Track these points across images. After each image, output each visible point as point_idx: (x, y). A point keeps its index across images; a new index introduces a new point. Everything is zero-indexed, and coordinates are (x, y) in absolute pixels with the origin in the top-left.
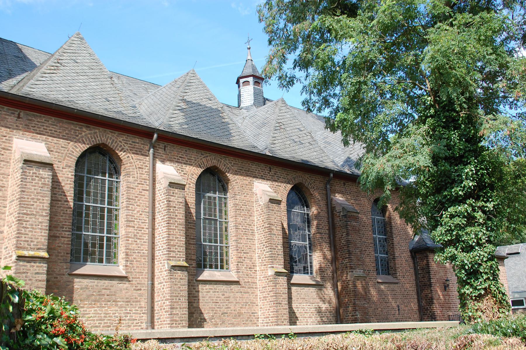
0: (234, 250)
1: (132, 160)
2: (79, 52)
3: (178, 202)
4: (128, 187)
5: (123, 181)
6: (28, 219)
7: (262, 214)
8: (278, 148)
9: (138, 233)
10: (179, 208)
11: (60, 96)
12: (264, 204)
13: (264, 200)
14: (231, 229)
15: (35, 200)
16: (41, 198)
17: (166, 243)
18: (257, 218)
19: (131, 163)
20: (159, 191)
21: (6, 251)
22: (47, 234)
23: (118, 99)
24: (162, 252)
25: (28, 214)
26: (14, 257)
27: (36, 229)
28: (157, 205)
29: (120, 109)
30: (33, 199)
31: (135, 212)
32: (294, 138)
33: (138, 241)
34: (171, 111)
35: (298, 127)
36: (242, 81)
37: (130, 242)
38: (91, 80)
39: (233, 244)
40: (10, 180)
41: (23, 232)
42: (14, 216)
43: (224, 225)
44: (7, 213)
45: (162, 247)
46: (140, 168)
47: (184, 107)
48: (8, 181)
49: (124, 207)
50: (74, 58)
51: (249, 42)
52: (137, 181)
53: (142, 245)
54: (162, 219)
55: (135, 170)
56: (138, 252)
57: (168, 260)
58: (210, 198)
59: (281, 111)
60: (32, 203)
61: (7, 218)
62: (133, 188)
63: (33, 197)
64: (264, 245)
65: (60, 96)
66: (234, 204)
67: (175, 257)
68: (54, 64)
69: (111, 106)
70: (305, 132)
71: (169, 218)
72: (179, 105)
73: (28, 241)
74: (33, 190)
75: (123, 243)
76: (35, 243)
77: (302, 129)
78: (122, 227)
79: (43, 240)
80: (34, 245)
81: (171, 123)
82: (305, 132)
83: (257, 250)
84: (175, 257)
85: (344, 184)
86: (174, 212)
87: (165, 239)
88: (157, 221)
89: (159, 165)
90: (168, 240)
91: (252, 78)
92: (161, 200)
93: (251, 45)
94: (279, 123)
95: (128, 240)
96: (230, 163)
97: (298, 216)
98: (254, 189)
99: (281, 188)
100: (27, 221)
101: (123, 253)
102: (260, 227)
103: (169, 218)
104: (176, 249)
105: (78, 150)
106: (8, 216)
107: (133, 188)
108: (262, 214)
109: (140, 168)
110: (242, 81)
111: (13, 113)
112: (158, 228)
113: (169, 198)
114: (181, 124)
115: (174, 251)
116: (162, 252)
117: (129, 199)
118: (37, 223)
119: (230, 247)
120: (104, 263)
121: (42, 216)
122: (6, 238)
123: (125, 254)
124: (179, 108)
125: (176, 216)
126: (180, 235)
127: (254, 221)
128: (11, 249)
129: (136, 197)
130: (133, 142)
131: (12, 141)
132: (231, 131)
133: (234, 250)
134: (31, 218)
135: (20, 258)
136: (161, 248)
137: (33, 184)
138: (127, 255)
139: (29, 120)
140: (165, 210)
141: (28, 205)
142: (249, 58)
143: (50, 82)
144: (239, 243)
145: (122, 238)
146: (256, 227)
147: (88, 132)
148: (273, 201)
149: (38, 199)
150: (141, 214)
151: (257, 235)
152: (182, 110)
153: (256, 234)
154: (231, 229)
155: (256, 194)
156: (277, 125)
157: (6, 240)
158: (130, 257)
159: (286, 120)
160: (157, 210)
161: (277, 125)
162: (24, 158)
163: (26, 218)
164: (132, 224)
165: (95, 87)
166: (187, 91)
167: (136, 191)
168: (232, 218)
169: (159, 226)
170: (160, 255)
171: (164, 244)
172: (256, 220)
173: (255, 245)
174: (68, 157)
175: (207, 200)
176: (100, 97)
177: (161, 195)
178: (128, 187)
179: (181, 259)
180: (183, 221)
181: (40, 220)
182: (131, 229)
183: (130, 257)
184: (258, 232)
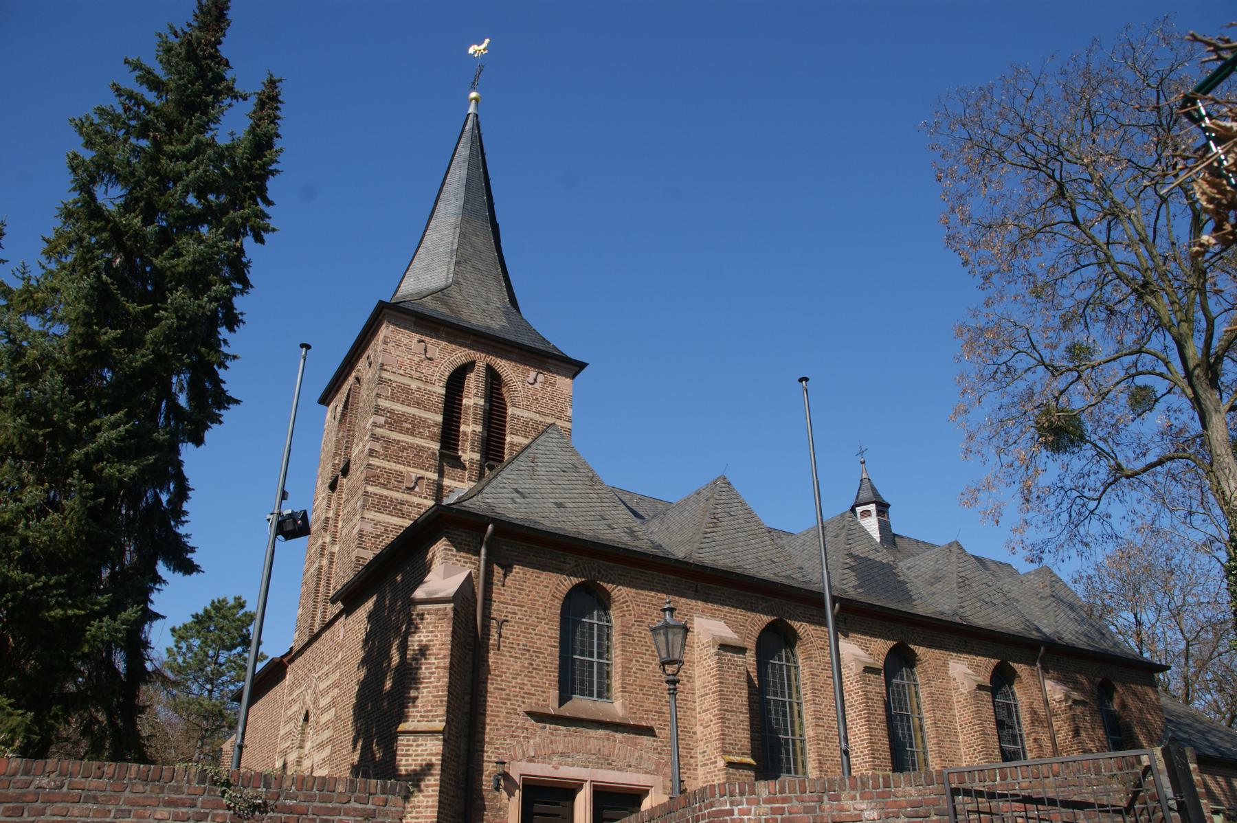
0: (936, 757)
1: (812, 639)
2: (731, 501)
3: (876, 692)
4: (812, 675)
5: (804, 666)
6: (729, 717)
7: (966, 706)
8: (969, 613)
9: (828, 734)
10: (877, 700)
11: (728, 561)
12: (968, 692)
13: (966, 687)
14: (928, 728)
15: (734, 693)
16: (739, 691)
17: (868, 747)
18: (959, 712)
19: (811, 642)
20: (847, 678)
21: (704, 757)
22: (748, 736)
23: (783, 559)
24: (863, 759)
25: (729, 711)
26: (721, 764)
27: (738, 729)
28: (846, 697)
29: (788, 573)
30: (731, 692)
31: (823, 706)
32: (983, 597)
33: (830, 744)
34: (840, 571)
35: (985, 581)
36: (859, 510)
37: (821, 746)
38: (751, 537)
39: (934, 748)
40: (696, 669)
41: (726, 732)
42: (711, 713)
43: (796, 708)
44: (698, 710)
45: (861, 752)
46: (821, 648)
47: (853, 564)
48: (694, 670)
49: (809, 700)
50: (728, 510)
51: (861, 453)
52: (820, 665)
53: (834, 750)
54: (857, 716)
55: (817, 652)
56: (832, 760)
57: (874, 769)
58: (898, 685)
59: (961, 561)
60: (731, 697)
61: (698, 716)
62: (817, 675)
63: (731, 689)
64: (974, 750)
65: (728, 561)
66: (928, 694)
67: (880, 766)
68: (711, 521)
69: (778, 570)
70: (994, 587)
71: (868, 713)
72: (847, 561)
73: (732, 744)
74: (730, 681)
75: (812, 747)
76: (739, 746)
77: (990, 584)
78: (808, 727)
79: (746, 743)
80: (739, 749)
81: (844, 587)
82: (994, 587)
83: (964, 757)
84: (880, 766)
85: (1058, 660)
86: (873, 706)
87: (718, 734)
88: (849, 718)
89: (843, 644)
90: (871, 743)
91: (874, 505)
92: (852, 691)
93: (866, 456)
94: (962, 577)
95: (819, 744)
96: (919, 637)
97: (1003, 707)
98: (950, 672)
99: (981, 669)
100: (729, 720)
101: (814, 760)
102: (966, 724)
103: (868, 713)
104: (881, 755)
105: (756, 628)
106: (699, 713)
107: (817, 675)
108: (966, 706)
109: (821, 648)
110: (859, 510)
111: (691, 587)
112: (852, 728)
113: (866, 687)
114: (855, 587)
115: (879, 758)
116: (863, 759)
117: (815, 689)
118: (739, 722)
119: (929, 753)
120: (793, 774)
121: (741, 712)
122: (702, 740)
123: (817, 762)
124: (848, 566)
125: (876, 711)
126: (883, 736)
127: (955, 716)
128: (713, 754)
129: (822, 687)
130: (811, 615)
131: (693, 620)
132: (911, 593)
133: (936, 757)
134: (732, 716)
135: (730, 764)
136: (859, 754)
137: (730, 673)
138: (820, 763)
139: (706, 593)
140: (862, 703)
141: (727, 699)
142: (864, 476)
143: (713, 544)
144: (941, 747)
145: (809, 741)
146: (958, 724)
147: (764, 605)
148: (868, 669)
149: (737, 692)
150: (829, 710)
151: (961, 738)
152: (851, 568)
153: (960, 734)
154: (928, 728)
155: (955, 679)
156: (960, 580)
157: (702, 743)
158: (824, 766)
159: (968, 572)
160: (847, 704)
161: (960, 580)
162: (719, 642)
163: (728, 715)
164: (821, 723)
165: (757, 546)
166: (850, 542)
167: (820, 680)
168: (927, 712)
169: (853, 724)
170: (860, 763)
171: (863, 748)
172: (957, 714)
173: (960, 749)
174: (748, 637)
175: (895, 688)
176: (764, 558)
177: (852, 683)
178: (812, 675)
179: (888, 769)
180: (883, 717)
181: (741, 718)
182: (820, 730)
183: (824, 766)
184: (962, 732)
